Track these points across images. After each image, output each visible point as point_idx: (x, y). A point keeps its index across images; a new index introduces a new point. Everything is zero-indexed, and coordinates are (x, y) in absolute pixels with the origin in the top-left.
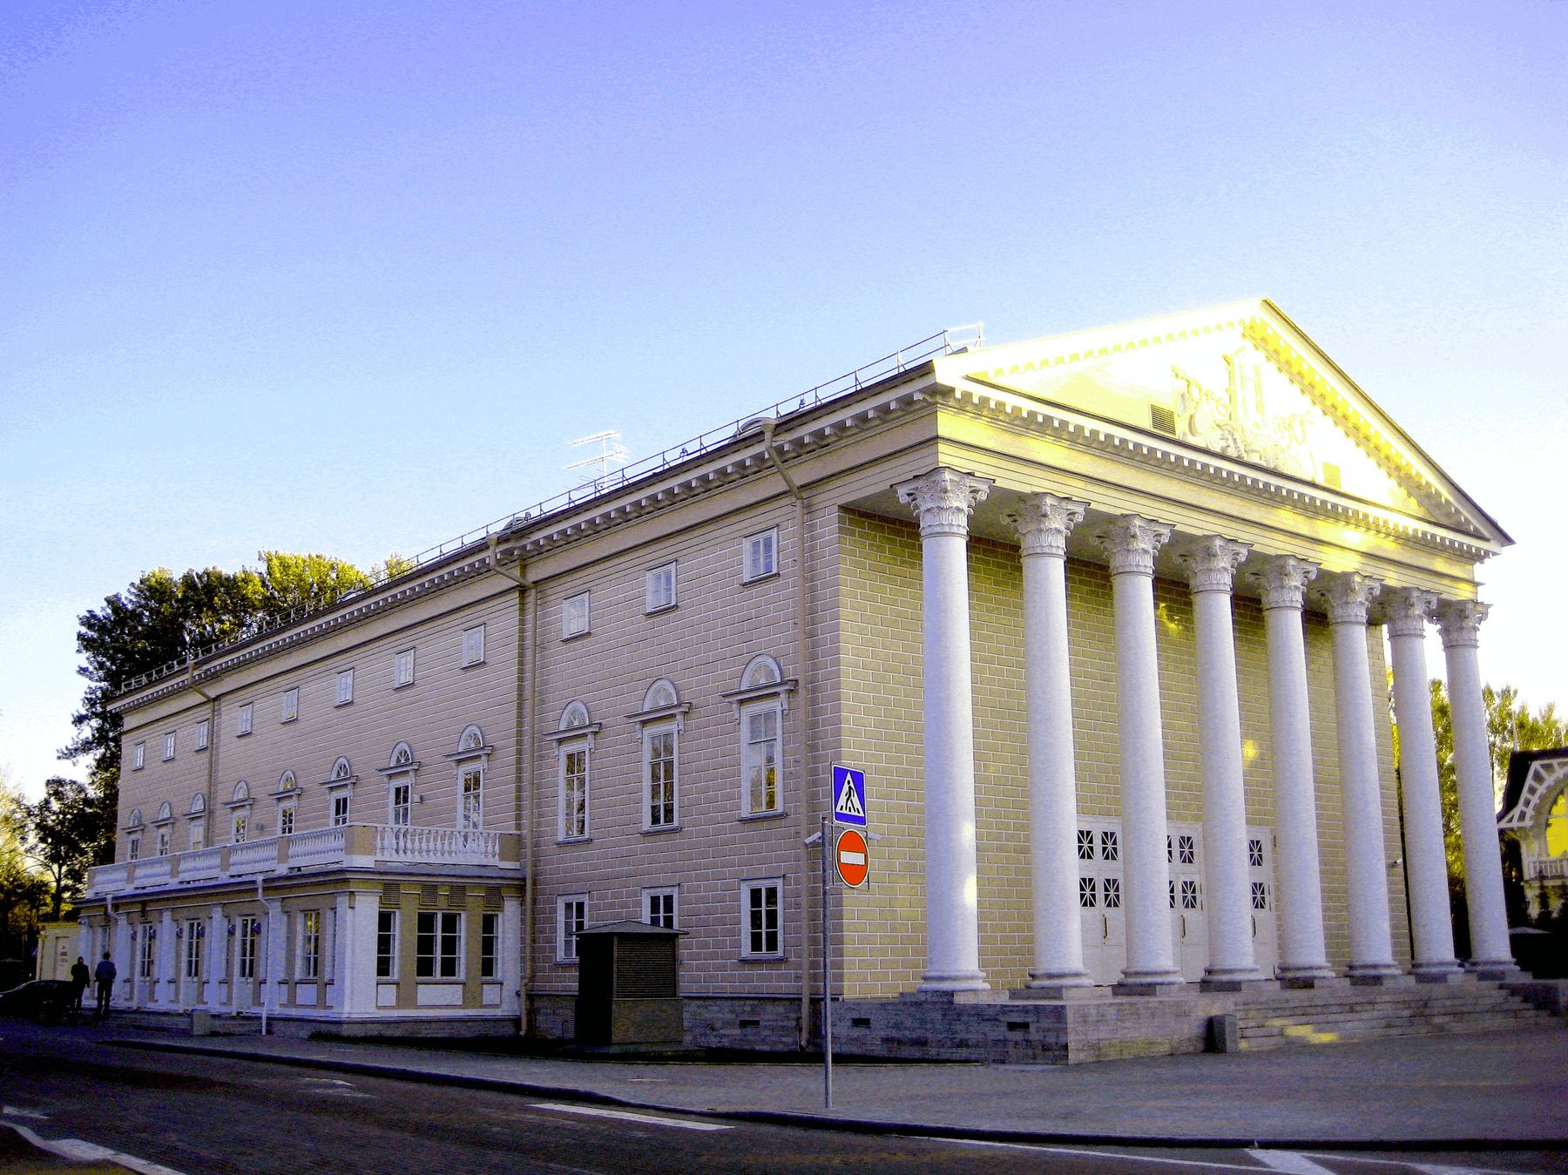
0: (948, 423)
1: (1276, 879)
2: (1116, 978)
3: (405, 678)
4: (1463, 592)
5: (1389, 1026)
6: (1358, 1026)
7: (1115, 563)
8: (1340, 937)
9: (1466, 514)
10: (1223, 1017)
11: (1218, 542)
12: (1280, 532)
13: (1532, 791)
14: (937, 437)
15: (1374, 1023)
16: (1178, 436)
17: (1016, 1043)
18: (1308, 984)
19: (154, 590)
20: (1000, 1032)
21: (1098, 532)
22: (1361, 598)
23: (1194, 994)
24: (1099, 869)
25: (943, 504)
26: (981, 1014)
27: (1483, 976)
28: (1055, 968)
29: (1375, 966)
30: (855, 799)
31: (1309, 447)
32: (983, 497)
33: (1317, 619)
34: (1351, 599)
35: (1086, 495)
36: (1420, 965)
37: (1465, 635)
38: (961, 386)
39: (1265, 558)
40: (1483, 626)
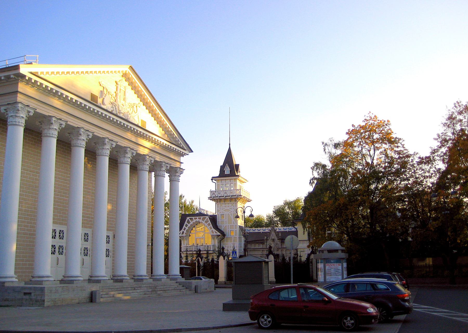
0: (22, 87)
1: (113, 248)
2: (61, 278)
4: (177, 165)
5: (145, 294)
6: (136, 294)
7: (73, 142)
8: (132, 265)
9: (181, 141)
10: (96, 291)
11: (107, 140)
12: (125, 139)
13: (186, 226)
14: (17, 92)
15: (141, 293)
16: (98, 104)
17: (26, 300)
18: (121, 281)
20: (21, 296)
21: (68, 132)
22: (148, 163)
23: (86, 284)
24: (58, 242)
25: (17, 115)
26: (14, 289)
27: (172, 279)
29: (141, 276)
31: (140, 116)
32: (31, 114)
33: (134, 169)
34: (126, 155)
35: (36, 106)
36: (153, 276)
37: (176, 178)
38: (29, 75)
39: (121, 147)
40: (182, 175)
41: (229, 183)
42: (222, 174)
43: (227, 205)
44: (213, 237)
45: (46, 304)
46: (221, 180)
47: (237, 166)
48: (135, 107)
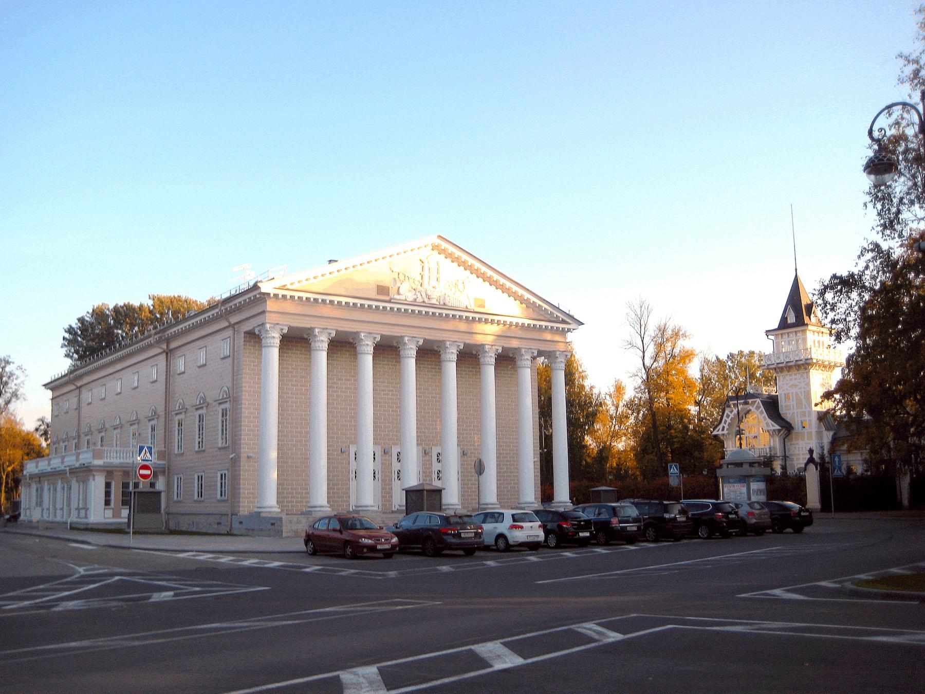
3: (202, 362)
9: (556, 313)
13: (728, 416)
19: (99, 314)
28: (363, 504)
30: (148, 454)
41: (794, 338)
42: (784, 324)
43: (793, 377)
45: (284, 534)
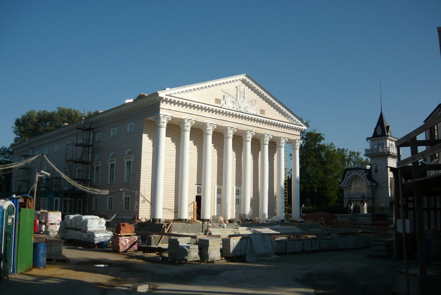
13: (347, 178)
34: (247, 136)
42: (375, 135)
44: (368, 187)
46: (378, 139)
47: (388, 127)
48: (254, 102)
